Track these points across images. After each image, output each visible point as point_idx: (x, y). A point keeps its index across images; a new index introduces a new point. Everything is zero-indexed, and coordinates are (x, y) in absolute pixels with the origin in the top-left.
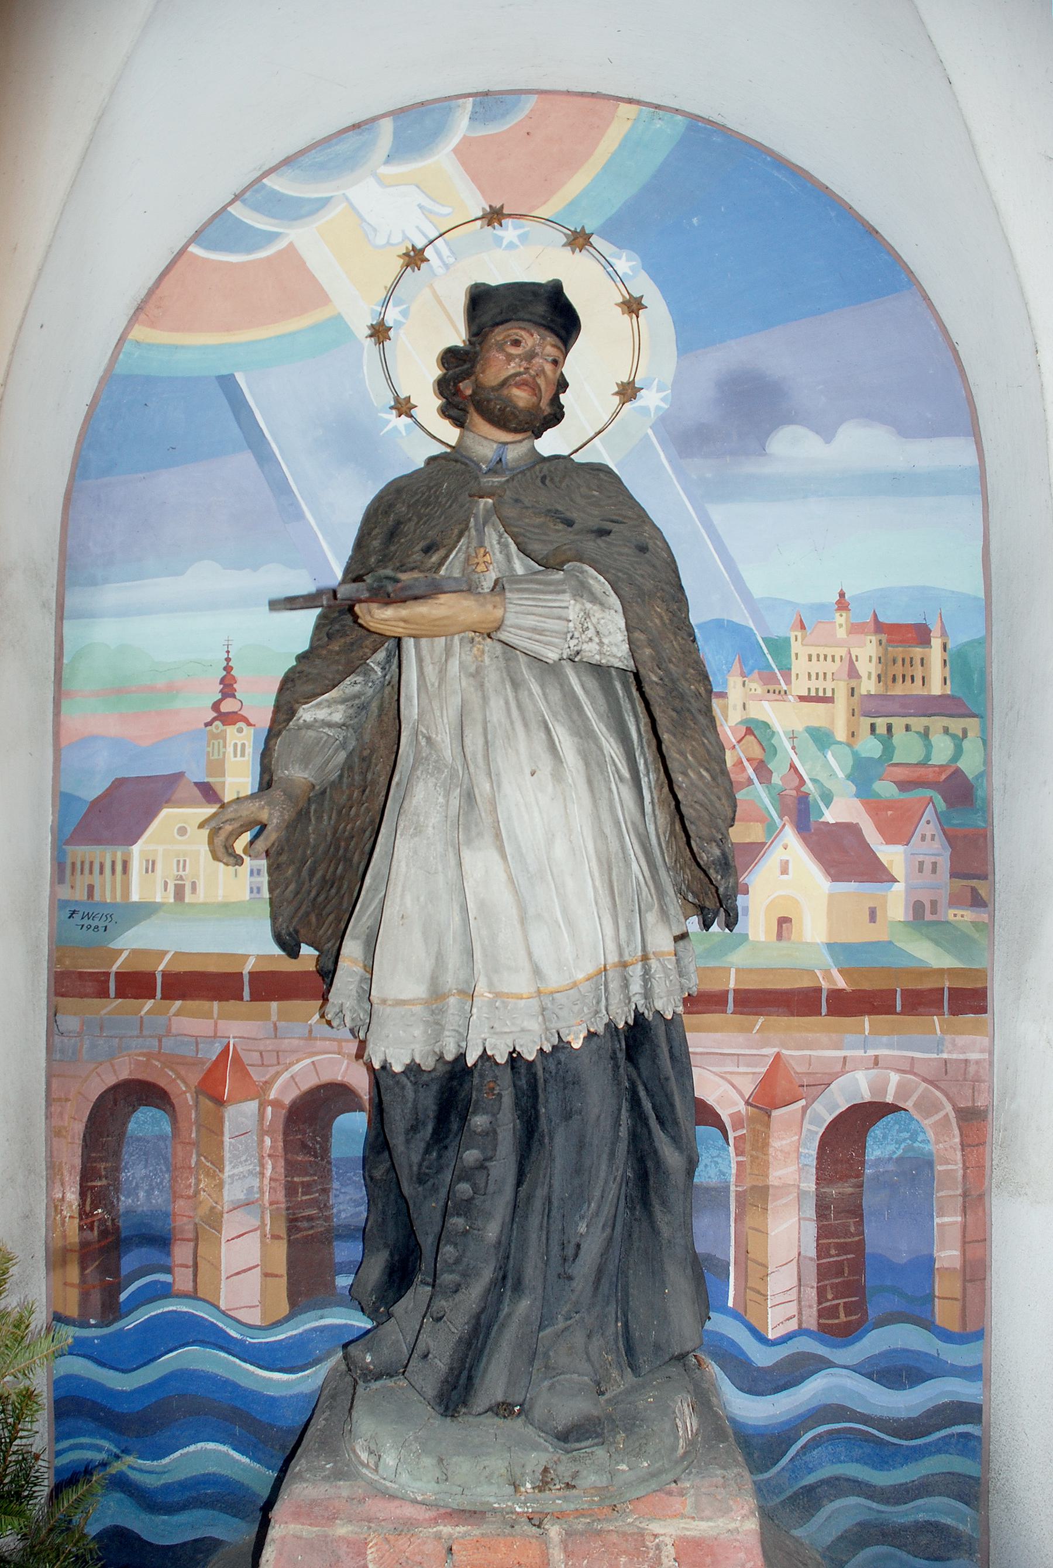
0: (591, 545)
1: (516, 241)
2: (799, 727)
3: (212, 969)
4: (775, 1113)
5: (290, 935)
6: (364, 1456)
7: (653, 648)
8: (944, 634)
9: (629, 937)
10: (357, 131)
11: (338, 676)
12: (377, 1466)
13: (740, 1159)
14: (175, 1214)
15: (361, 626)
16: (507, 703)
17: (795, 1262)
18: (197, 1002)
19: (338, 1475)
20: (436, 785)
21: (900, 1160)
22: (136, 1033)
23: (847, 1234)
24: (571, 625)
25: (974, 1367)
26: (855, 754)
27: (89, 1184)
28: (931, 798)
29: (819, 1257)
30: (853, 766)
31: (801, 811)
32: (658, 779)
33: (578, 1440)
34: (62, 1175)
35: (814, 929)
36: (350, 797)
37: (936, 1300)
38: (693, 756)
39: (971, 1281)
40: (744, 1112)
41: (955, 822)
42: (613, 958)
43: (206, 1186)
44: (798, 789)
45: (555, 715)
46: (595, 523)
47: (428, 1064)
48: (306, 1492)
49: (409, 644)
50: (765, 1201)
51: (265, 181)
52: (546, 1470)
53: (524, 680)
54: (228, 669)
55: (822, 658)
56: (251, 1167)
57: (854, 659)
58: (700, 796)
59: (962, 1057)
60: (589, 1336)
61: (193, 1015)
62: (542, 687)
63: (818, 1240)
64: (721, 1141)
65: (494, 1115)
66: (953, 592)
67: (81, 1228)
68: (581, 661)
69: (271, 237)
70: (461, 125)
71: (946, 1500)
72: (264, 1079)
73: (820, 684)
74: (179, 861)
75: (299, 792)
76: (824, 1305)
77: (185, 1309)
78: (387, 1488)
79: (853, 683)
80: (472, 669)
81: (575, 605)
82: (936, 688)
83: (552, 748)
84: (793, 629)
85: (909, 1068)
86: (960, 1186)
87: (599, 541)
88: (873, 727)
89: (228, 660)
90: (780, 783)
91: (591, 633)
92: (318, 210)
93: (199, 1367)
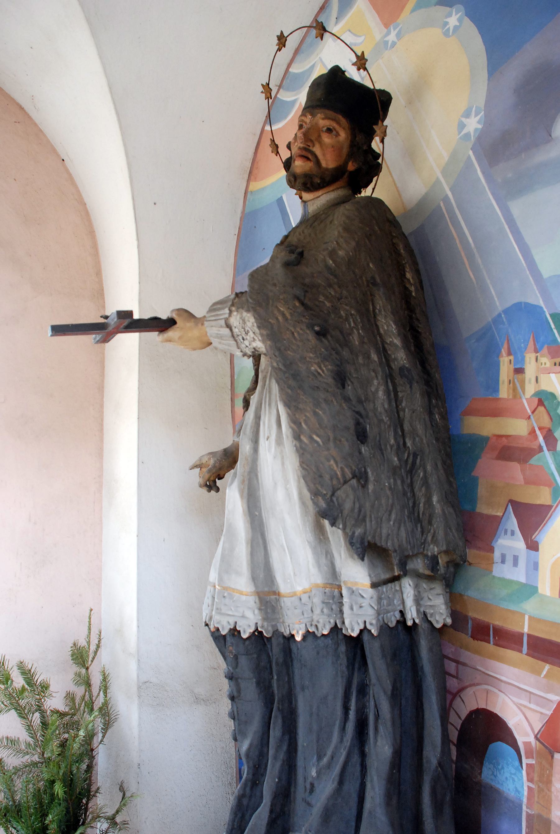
38: (306, 424)
64: (517, 763)
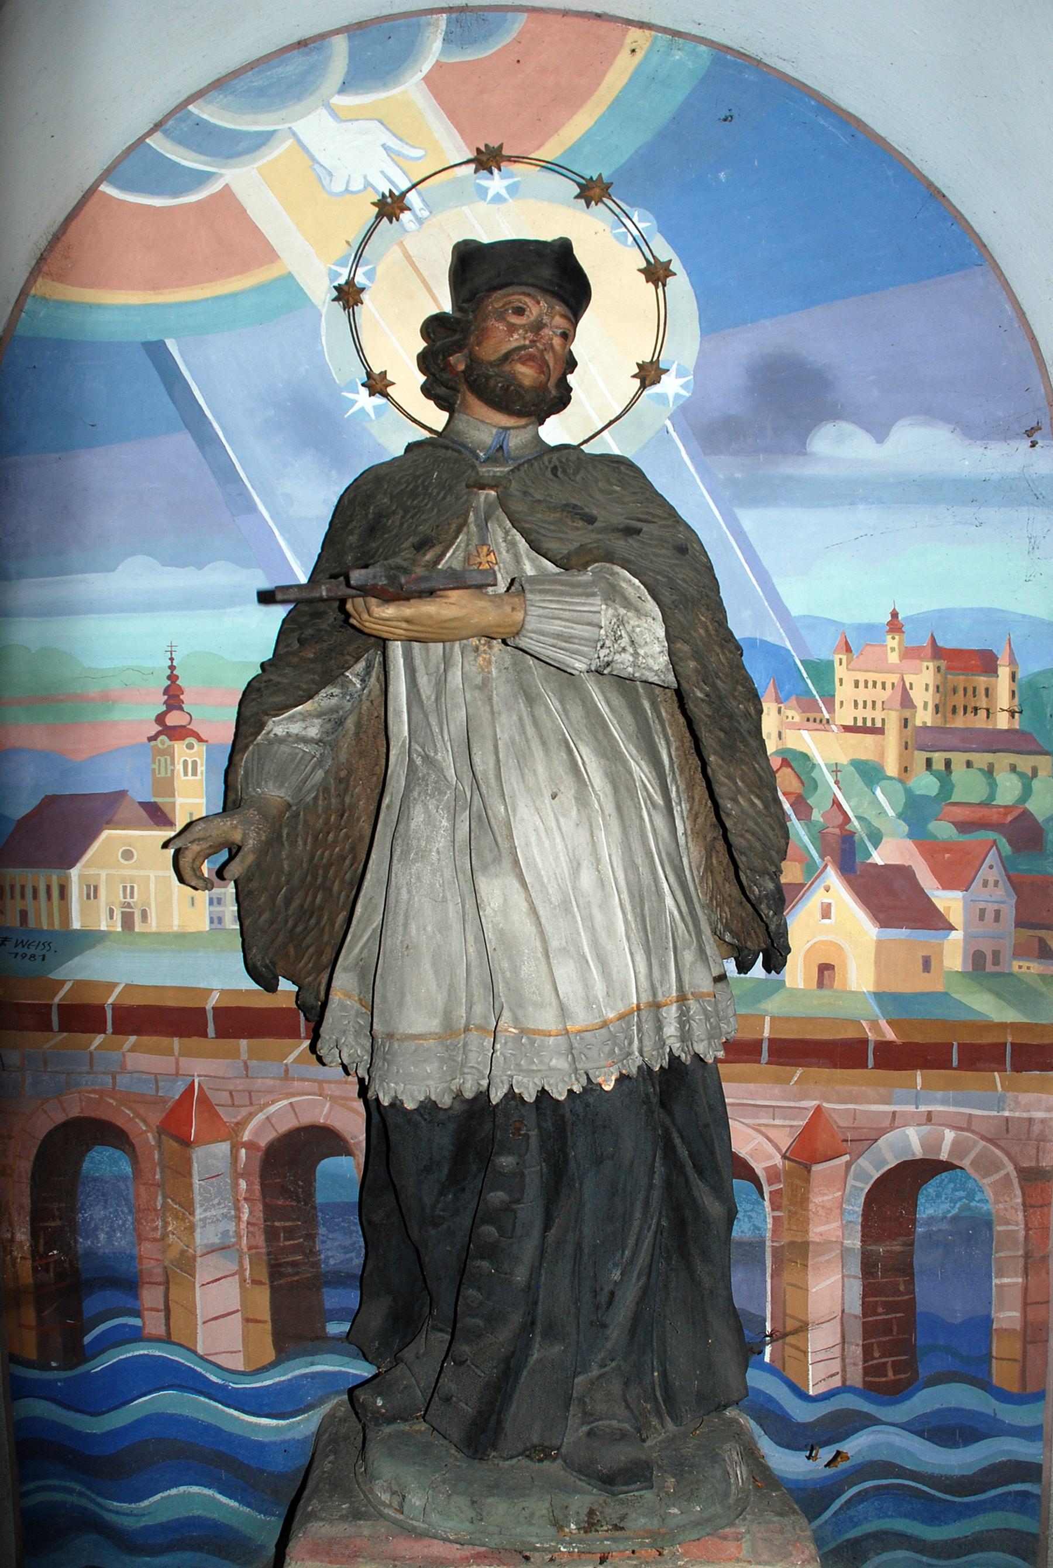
0: (621, 545)
1: (504, 193)
2: (844, 760)
3: (170, 1003)
4: (816, 1168)
5: (266, 966)
6: (385, 1497)
7: (697, 660)
8: (1013, 662)
9: (662, 975)
10: (303, 50)
11: (313, 686)
12: (401, 1506)
13: (777, 1214)
14: (141, 1258)
15: (353, 626)
16: (521, 719)
17: (838, 1319)
18: (155, 1038)
19: (356, 1515)
20: (438, 808)
21: (955, 1219)
22: (86, 1068)
23: (896, 1292)
24: (603, 632)
25: (1033, 1427)
26: (908, 792)
27: (42, 1224)
28: (995, 842)
29: (864, 1315)
30: (905, 804)
31: (845, 852)
32: (691, 809)
33: (626, 1483)
34: (10, 1214)
35: (860, 977)
36: (327, 822)
37: (994, 1360)
38: (743, 781)
39: (1030, 1343)
40: (780, 1165)
41: (1021, 867)
42: (646, 998)
43: (175, 1229)
44: (841, 827)
45: (578, 733)
46: (619, 520)
47: (445, 1102)
48: (323, 1530)
49: (397, 650)
50: (805, 1256)
51: (191, 107)
52: (591, 1513)
53: (539, 695)
54: (173, 678)
55: (870, 684)
56: (225, 1210)
57: (908, 687)
58: (751, 824)
59: (1025, 1115)
60: (626, 1384)
61: (150, 1051)
62: (562, 702)
63: (863, 1298)
64: (756, 1196)
65: (521, 1156)
66: (1024, 616)
67: (35, 1269)
68: (610, 674)
69: (202, 178)
70: (434, 49)
71: (1000, 1554)
72: (235, 1120)
73: (869, 714)
74: (125, 888)
75: (275, 811)
76: (870, 1363)
77: (157, 1353)
78: (415, 1527)
79: (907, 713)
80: (478, 680)
81: (607, 609)
82: (1003, 722)
83: (574, 769)
84: (837, 651)
85: (966, 1125)
86: (1021, 1246)
87: (630, 540)
88: (929, 763)
89: (172, 668)
90: (822, 820)
91: (625, 642)
92: (264, 144)
93: (178, 1412)
